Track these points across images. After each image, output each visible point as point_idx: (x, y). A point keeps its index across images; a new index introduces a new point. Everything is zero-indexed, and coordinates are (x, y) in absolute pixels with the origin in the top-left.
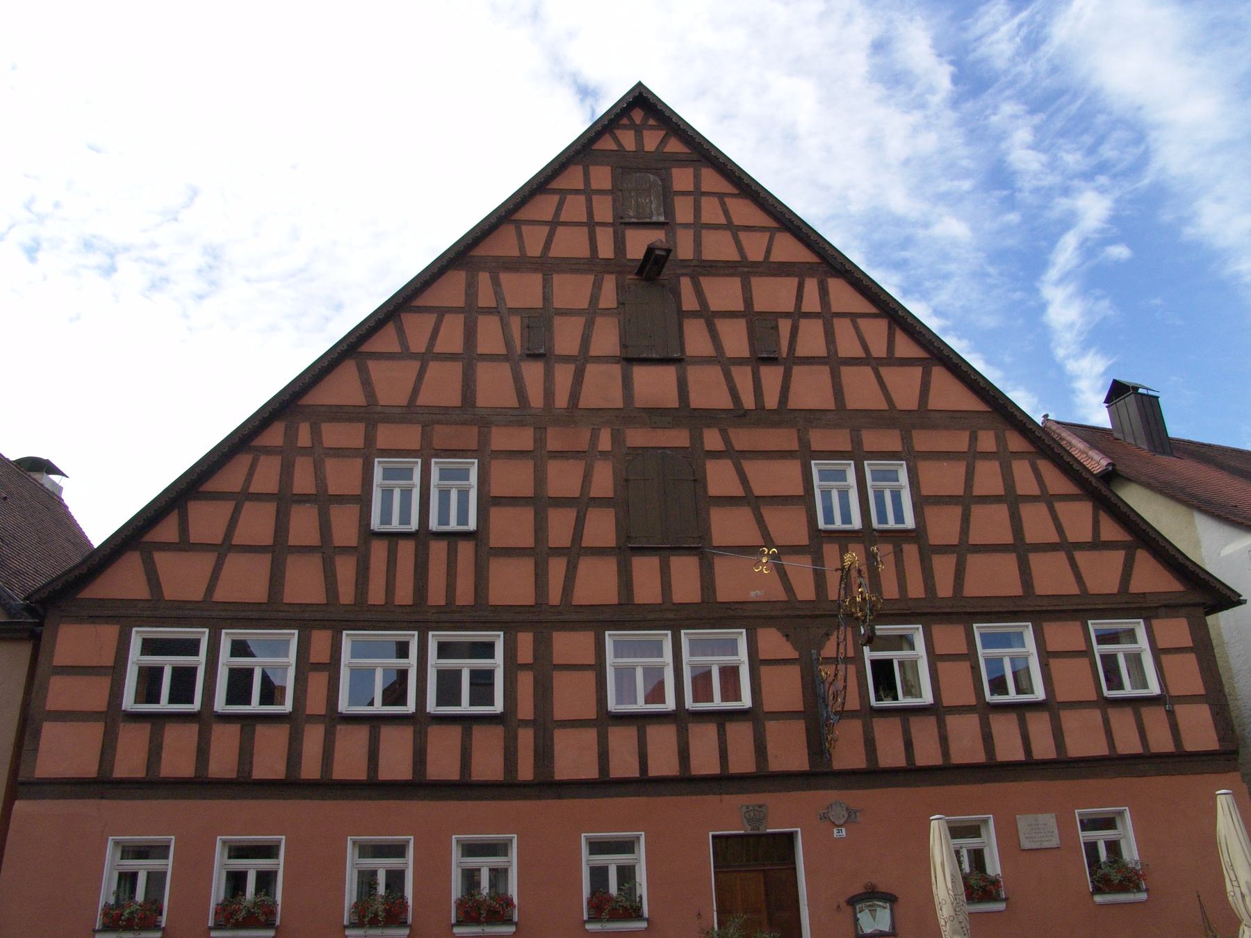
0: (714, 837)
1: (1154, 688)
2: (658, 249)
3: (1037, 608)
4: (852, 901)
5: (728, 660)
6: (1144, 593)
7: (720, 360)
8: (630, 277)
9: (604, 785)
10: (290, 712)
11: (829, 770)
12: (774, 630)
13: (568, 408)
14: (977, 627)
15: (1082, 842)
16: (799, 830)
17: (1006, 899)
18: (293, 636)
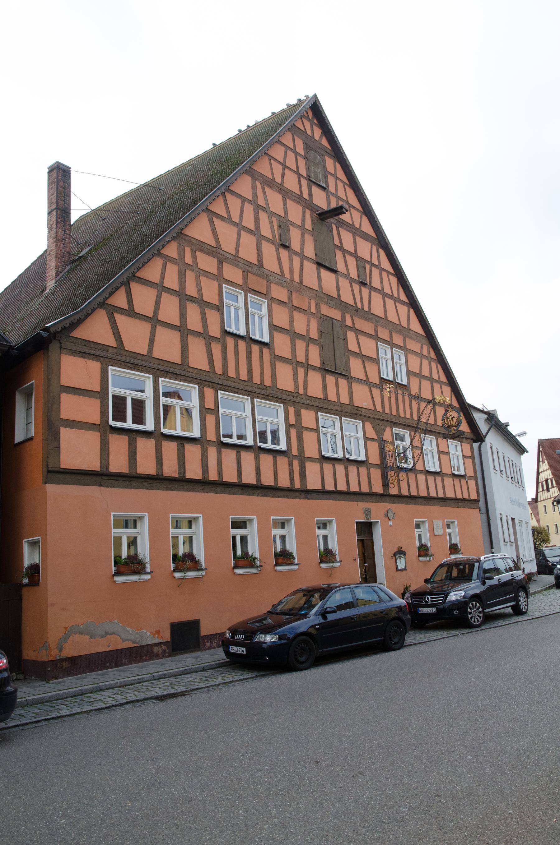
1: (196, 433)
5: (139, 395)
7: (256, 232)
9: (322, 493)
14: (112, 370)
15: (113, 536)
16: (170, 515)
17: (340, 561)
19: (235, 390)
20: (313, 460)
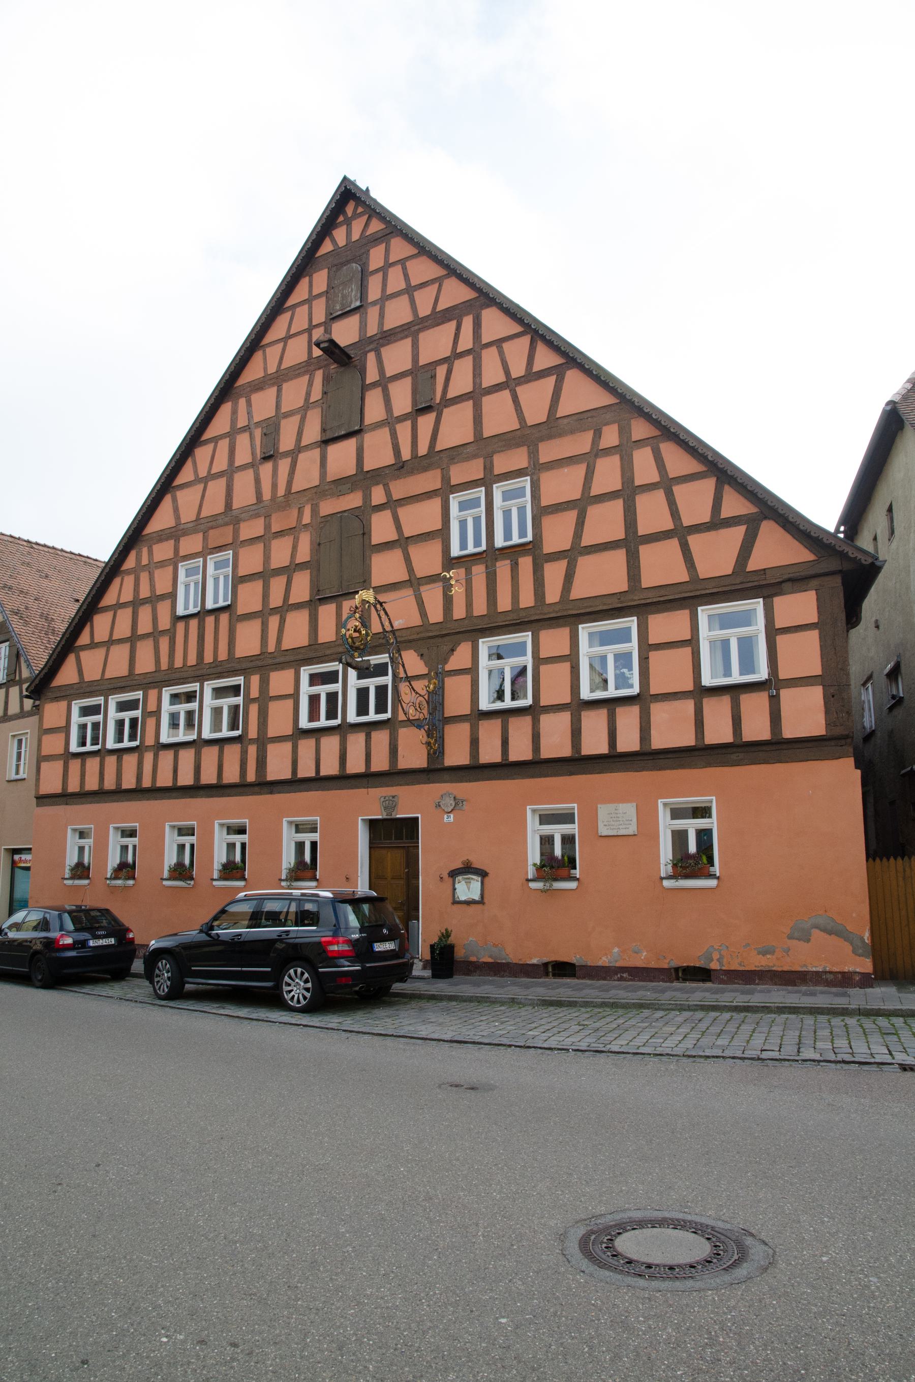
0: (417, 819)
2: (322, 342)
3: (643, 602)
4: (454, 874)
6: (764, 570)
8: (332, 367)
9: (295, 783)
10: (766, 680)
11: (442, 766)
12: (412, 651)
13: (285, 495)
18: (758, 605)
19: (182, 681)
20: (282, 738)
